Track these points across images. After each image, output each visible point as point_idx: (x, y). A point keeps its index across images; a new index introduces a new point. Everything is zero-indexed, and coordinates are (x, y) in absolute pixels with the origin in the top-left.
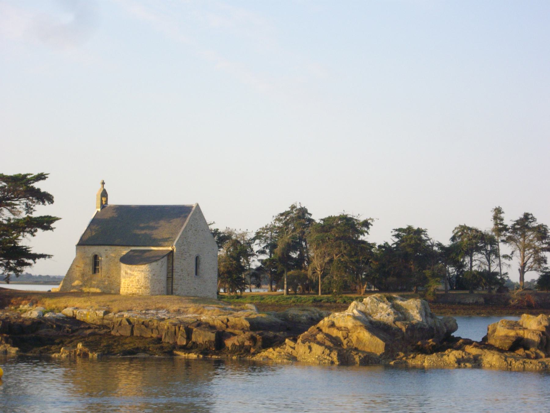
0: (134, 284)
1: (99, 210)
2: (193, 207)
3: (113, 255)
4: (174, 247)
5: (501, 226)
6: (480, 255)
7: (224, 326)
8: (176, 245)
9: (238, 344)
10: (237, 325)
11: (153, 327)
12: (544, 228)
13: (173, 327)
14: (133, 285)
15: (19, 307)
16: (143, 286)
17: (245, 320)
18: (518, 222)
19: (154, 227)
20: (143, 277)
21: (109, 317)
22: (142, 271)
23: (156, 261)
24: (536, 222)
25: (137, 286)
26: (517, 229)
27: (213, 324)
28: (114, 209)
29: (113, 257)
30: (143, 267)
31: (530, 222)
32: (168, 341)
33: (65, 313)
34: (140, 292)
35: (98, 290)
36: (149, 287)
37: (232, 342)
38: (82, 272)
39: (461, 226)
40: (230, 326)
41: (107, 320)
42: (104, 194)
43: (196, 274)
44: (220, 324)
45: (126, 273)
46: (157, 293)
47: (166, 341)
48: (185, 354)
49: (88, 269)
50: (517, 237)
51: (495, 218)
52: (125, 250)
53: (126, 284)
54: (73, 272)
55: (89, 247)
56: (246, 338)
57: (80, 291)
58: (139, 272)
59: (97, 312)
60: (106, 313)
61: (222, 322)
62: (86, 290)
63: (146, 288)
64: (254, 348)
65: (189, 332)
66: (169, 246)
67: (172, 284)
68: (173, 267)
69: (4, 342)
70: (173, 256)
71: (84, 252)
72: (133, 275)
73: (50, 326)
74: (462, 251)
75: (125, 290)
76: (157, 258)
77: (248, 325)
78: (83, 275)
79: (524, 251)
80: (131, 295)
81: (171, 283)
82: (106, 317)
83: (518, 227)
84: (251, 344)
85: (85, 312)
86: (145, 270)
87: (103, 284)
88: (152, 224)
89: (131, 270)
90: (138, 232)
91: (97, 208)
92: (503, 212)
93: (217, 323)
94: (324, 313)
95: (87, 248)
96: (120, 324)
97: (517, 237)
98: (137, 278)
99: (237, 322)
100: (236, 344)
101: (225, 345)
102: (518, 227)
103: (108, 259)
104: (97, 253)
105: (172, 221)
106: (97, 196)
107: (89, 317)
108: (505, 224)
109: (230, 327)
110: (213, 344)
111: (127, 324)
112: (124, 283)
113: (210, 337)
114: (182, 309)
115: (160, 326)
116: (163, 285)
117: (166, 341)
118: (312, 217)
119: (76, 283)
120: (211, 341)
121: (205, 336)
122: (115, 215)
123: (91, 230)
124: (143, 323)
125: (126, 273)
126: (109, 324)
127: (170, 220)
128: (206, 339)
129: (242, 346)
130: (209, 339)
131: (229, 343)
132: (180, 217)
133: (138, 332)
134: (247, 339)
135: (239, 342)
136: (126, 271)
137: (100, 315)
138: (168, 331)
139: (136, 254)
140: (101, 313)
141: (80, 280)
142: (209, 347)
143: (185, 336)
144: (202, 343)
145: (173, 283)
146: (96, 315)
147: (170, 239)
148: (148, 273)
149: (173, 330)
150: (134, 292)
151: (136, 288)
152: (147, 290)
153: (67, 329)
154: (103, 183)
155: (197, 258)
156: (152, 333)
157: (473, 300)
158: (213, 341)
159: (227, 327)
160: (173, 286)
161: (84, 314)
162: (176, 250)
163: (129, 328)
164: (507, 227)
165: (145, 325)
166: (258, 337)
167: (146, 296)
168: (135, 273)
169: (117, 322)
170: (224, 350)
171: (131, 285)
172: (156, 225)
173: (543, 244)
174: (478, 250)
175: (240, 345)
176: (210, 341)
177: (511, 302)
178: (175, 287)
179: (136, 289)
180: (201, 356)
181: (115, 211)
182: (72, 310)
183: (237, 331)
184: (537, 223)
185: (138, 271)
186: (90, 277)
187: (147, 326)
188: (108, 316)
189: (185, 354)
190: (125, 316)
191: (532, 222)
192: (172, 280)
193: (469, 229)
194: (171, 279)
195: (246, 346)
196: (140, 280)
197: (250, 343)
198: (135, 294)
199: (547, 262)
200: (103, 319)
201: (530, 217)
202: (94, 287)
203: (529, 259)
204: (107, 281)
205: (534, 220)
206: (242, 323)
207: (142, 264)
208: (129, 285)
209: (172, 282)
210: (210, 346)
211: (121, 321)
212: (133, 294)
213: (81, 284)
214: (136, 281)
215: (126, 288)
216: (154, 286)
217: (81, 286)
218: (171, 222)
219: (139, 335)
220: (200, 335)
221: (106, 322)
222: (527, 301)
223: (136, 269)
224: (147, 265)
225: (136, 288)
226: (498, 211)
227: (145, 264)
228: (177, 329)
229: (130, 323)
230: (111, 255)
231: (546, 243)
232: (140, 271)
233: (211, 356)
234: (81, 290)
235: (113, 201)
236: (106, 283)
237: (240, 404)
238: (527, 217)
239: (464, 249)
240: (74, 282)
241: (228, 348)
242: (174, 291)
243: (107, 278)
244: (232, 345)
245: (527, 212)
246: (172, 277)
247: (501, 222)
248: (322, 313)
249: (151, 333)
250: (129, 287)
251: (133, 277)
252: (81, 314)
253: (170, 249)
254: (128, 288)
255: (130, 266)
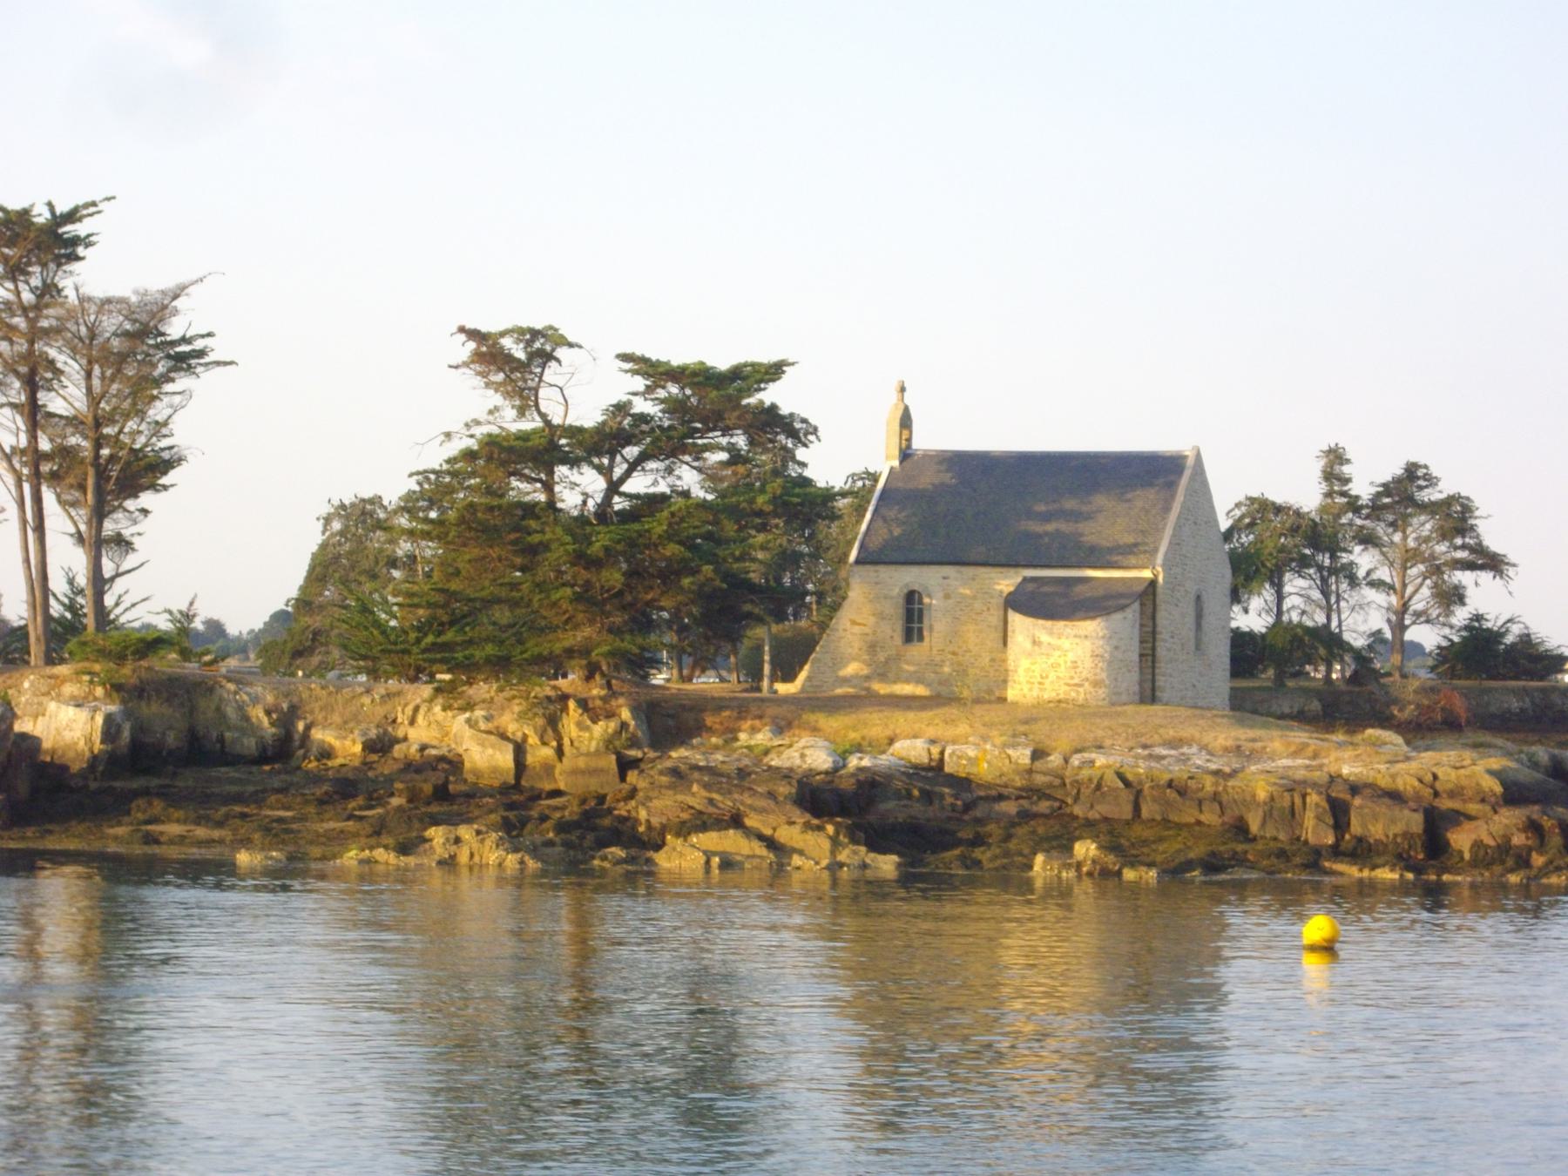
0: (1062, 672)
1: (896, 463)
2: (1186, 457)
3: (968, 592)
4: (1160, 569)
5: (1345, 500)
6: (1301, 583)
7: (1428, 792)
8: (1163, 566)
9: (1492, 843)
10: (1463, 788)
11: (1200, 795)
12: (1462, 505)
13: (1286, 794)
14: (1058, 677)
15: (736, 739)
16: (1087, 679)
17: (1487, 777)
18: (1387, 489)
19: (1081, 513)
20: (1088, 655)
21: (1050, 766)
22: (1086, 637)
23: (1122, 608)
24: (1438, 488)
25: (1072, 678)
26: (1386, 507)
27: (1393, 786)
28: (940, 463)
29: (964, 596)
30: (1092, 627)
31: (1421, 488)
32: (1274, 833)
33: (904, 754)
34: (1080, 695)
35: (921, 690)
36: (1103, 681)
37: (1474, 836)
38: (870, 638)
39: (1252, 500)
40: (1445, 791)
41: (1045, 774)
42: (906, 421)
43: (1198, 647)
44: (1414, 788)
45: (1035, 642)
46: (1124, 698)
47: (1268, 835)
48: (1361, 870)
49: (889, 632)
50: (1381, 529)
51: (1330, 476)
52: (1006, 578)
53: (1037, 674)
54: (841, 638)
55: (893, 568)
56: (1515, 825)
57: (863, 693)
58: (1078, 640)
59: (1010, 752)
60: (1038, 754)
61: (1421, 781)
62: (882, 688)
63: (1096, 684)
64: (1541, 854)
65: (1338, 813)
66: (1143, 567)
67: (1154, 675)
68: (1154, 625)
69: (846, 840)
70: (1154, 594)
71: (877, 583)
72: (1058, 648)
73: (904, 792)
74: (1263, 570)
75: (1031, 690)
76: (1123, 602)
77: (1498, 789)
78: (872, 647)
79: (1405, 569)
80: (1051, 705)
81: (1150, 671)
82: (1038, 765)
83: (1387, 500)
84: (1530, 842)
85: (972, 753)
86: (1094, 634)
87: (936, 673)
88: (1070, 504)
89: (1051, 633)
90: (1038, 528)
91: (887, 458)
92: (1348, 461)
93: (1405, 784)
94: (1541, 754)
95: (885, 572)
96: (1099, 787)
97: (1381, 529)
98: (1071, 656)
99: (1464, 782)
100: (1485, 841)
101: (1447, 844)
102: (1387, 500)
103: (951, 601)
104: (916, 588)
105: (1129, 496)
106: (888, 424)
107: (986, 765)
108: (1353, 493)
109: (1445, 796)
110: (1419, 844)
111: (1121, 785)
112: (1027, 670)
113: (1407, 825)
114: (1247, 746)
115: (1228, 794)
116: (1131, 680)
117: (1268, 835)
118: (807, 473)
119: (851, 669)
120: (1412, 835)
121: (1393, 821)
122: (947, 478)
123: (885, 520)
124: (1170, 784)
125: (1035, 642)
126: (1050, 786)
127: (1122, 494)
128: (1398, 828)
129: (1504, 848)
130: (1404, 828)
131: (1461, 840)
132: (1151, 485)
133: (1156, 807)
134: (1518, 829)
135: (1494, 838)
136: (1034, 636)
137: (1020, 761)
138: (1272, 807)
139: (1046, 589)
140: (1023, 756)
141: (864, 662)
142: (1408, 852)
143: (1331, 821)
144: (1384, 839)
145: (1157, 671)
146: (1007, 761)
147: (1141, 548)
148: (1101, 643)
149: (1286, 803)
150: (1062, 696)
151: (1068, 685)
152: (1101, 691)
153: (949, 800)
154: (903, 390)
155: (1198, 598)
156: (1201, 811)
157: (1291, 707)
158: (1419, 835)
159: (1436, 794)
160: (1157, 677)
161: (969, 759)
162: (1164, 578)
163: (1126, 797)
164: (1360, 503)
165: (1179, 789)
166: (1547, 823)
167: (1098, 706)
168: (1066, 643)
169: (1090, 780)
170: (1448, 859)
171: (1052, 676)
172: (1084, 508)
173: (1456, 548)
174: (1304, 563)
175: (1499, 846)
176: (1406, 835)
177: (1396, 712)
178: (1161, 681)
179: (1067, 688)
180: (1410, 876)
181: (943, 468)
182: (926, 746)
183: (1473, 808)
184: (1440, 492)
185: (1075, 636)
186: (894, 652)
187: (1182, 792)
188: (1047, 762)
189: (1361, 870)
190: (1098, 764)
191: (1426, 487)
192: (1153, 662)
193: (1278, 509)
194: (1150, 658)
195: (1517, 847)
196: (1079, 663)
197: (1527, 838)
198: (1066, 701)
199: (1467, 600)
200: (1030, 771)
201: (1420, 472)
202: (907, 681)
203: (1416, 591)
204: (948, 663)
205: (1431, 481)
206: (1478, 784)
207: (1085, 619)
208: (1047, 677)
209: (1153, 668)
210: (1410, 847)
211: (1101, 778)
212: (1060, 701)
213: (866, 671)
214: (1069, 664)
215: (1037, 686)
216: (1116, 680)
217: (868, 678)
218: (1129, 501)
219: (1158, 818)
220: (1375, 818)
221: (1040, 779)
222: (1443, 709)
223: (1068, 630)
224: (1099, 620)
225: (1068, 685)
226: (1335, 457)
227: (1093, 618)
228: (1298, 801)
229: (1127, 783)
230: (962, 590)
231: (1464, 547)
232: (1080, 637)
233: (1439, 876)
234: (868, 689)
235: (926, 440)
236: (947, 669)
237: (930, 997)
238: (1413, 473)
239: (1269, 565)
240: (845, 666)
241: (1461, 853)
242: (1158, 694)
243: (950, 656)
244: (1473, 846)
245: (1413, 460)
246: (1154, 655)
247: (1346, 488)
248: (1533, 754)
249: (1196, 813)
250: (1047, 682)
251: (1057, 653)
252: (960, 757)
253: (1147, 574)
254: (1040, 683)
255: (1049, 623)
